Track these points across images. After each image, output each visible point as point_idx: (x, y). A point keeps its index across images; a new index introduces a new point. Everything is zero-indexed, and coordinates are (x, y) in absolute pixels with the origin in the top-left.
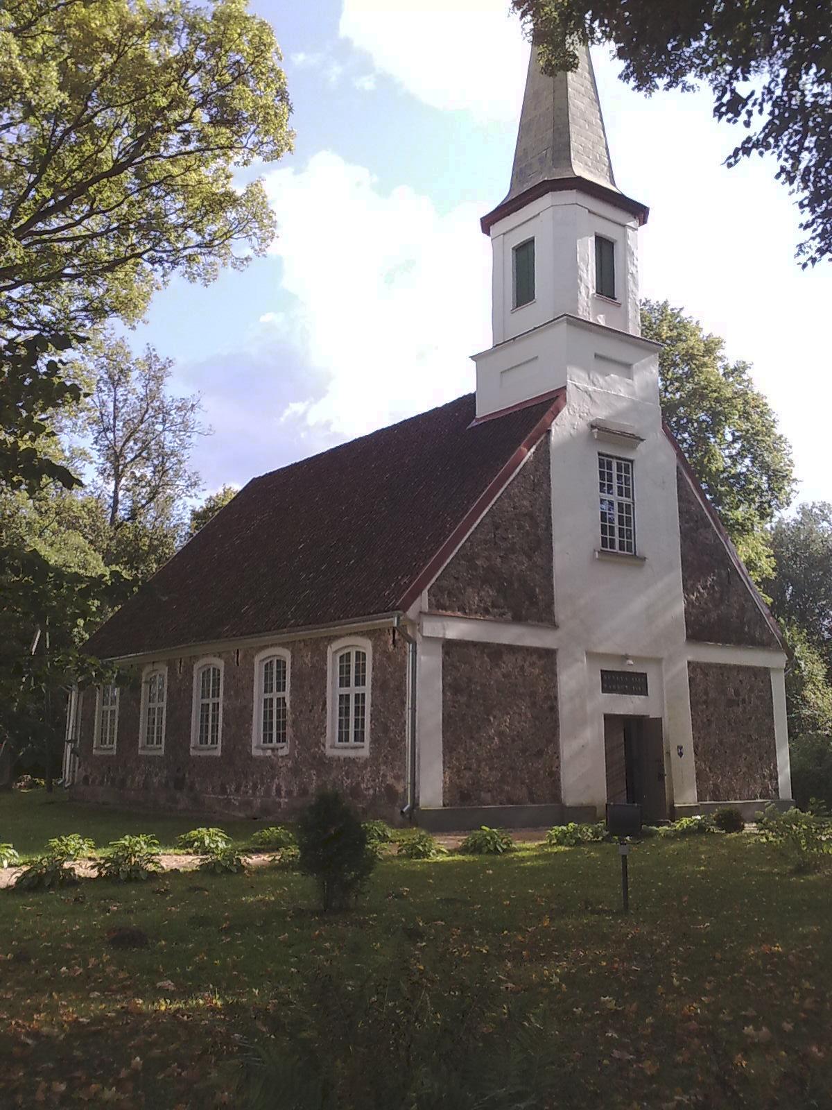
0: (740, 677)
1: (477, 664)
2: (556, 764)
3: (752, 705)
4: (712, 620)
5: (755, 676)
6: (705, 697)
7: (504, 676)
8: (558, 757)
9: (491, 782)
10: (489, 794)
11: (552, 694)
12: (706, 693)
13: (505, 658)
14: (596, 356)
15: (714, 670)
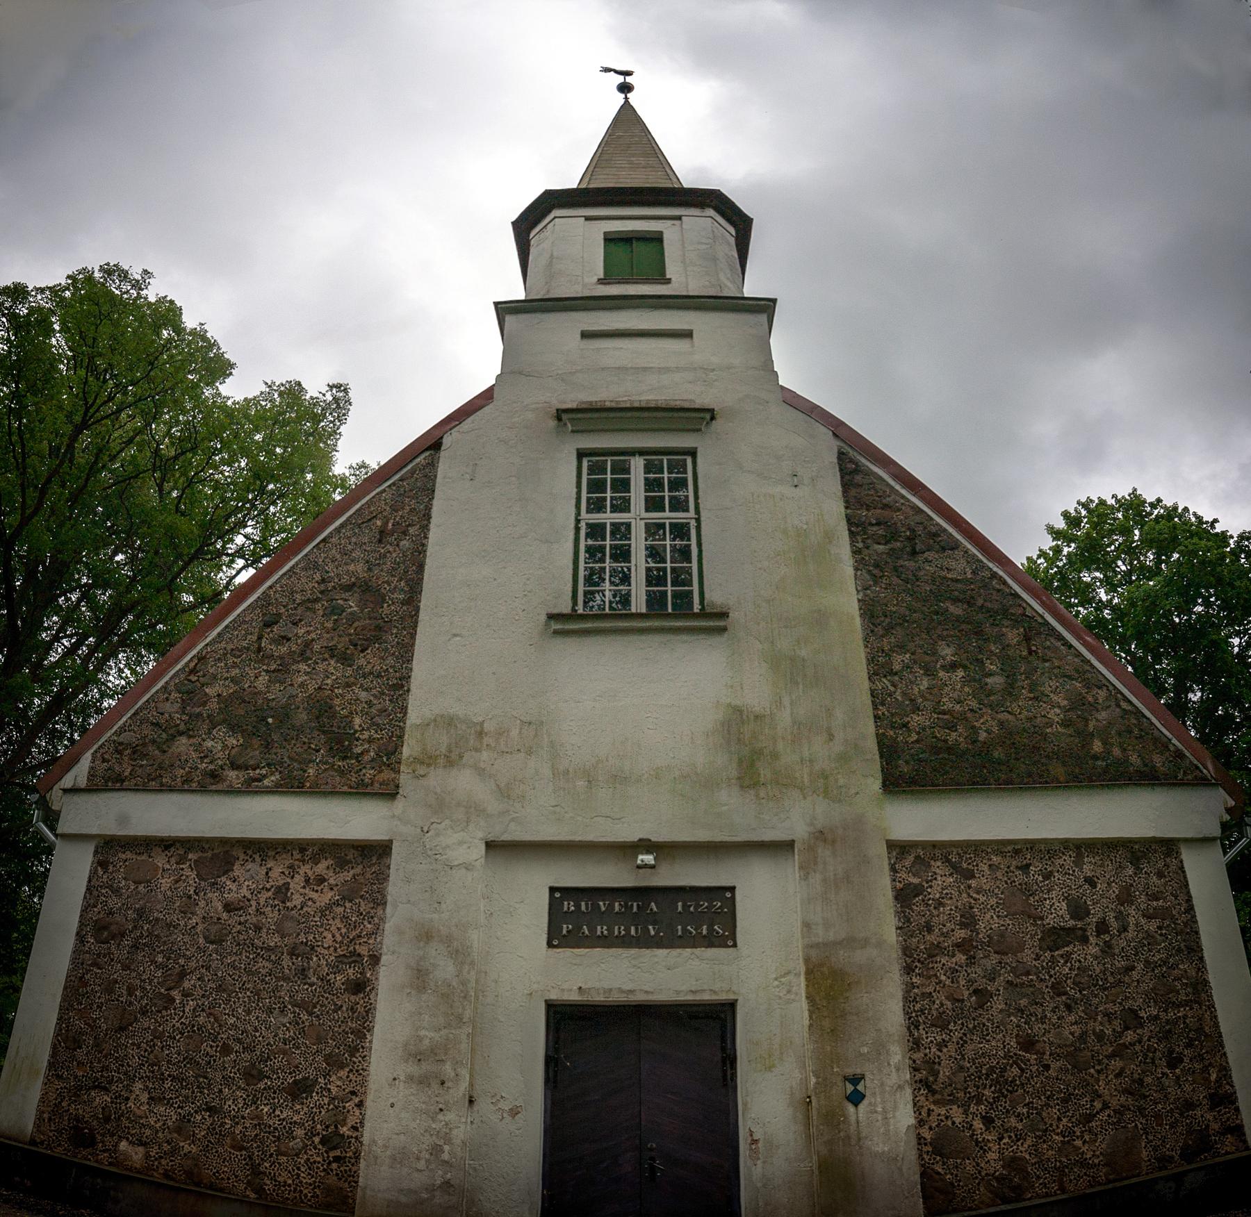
0: (1088, 870)
1: (166, 883)
2: (351, 1121)
3: (1131, 934)
4: (983, 736)
5: (1135, 860)
6: (961, 934)
7: (228, 907)
8: (360, 1105)
9: (151, 1127)
10: (141, 1149)
11: (363, 950)
12: (968, 921)
13: (237, 871)
14: (490, 845)
15: (996, 859)
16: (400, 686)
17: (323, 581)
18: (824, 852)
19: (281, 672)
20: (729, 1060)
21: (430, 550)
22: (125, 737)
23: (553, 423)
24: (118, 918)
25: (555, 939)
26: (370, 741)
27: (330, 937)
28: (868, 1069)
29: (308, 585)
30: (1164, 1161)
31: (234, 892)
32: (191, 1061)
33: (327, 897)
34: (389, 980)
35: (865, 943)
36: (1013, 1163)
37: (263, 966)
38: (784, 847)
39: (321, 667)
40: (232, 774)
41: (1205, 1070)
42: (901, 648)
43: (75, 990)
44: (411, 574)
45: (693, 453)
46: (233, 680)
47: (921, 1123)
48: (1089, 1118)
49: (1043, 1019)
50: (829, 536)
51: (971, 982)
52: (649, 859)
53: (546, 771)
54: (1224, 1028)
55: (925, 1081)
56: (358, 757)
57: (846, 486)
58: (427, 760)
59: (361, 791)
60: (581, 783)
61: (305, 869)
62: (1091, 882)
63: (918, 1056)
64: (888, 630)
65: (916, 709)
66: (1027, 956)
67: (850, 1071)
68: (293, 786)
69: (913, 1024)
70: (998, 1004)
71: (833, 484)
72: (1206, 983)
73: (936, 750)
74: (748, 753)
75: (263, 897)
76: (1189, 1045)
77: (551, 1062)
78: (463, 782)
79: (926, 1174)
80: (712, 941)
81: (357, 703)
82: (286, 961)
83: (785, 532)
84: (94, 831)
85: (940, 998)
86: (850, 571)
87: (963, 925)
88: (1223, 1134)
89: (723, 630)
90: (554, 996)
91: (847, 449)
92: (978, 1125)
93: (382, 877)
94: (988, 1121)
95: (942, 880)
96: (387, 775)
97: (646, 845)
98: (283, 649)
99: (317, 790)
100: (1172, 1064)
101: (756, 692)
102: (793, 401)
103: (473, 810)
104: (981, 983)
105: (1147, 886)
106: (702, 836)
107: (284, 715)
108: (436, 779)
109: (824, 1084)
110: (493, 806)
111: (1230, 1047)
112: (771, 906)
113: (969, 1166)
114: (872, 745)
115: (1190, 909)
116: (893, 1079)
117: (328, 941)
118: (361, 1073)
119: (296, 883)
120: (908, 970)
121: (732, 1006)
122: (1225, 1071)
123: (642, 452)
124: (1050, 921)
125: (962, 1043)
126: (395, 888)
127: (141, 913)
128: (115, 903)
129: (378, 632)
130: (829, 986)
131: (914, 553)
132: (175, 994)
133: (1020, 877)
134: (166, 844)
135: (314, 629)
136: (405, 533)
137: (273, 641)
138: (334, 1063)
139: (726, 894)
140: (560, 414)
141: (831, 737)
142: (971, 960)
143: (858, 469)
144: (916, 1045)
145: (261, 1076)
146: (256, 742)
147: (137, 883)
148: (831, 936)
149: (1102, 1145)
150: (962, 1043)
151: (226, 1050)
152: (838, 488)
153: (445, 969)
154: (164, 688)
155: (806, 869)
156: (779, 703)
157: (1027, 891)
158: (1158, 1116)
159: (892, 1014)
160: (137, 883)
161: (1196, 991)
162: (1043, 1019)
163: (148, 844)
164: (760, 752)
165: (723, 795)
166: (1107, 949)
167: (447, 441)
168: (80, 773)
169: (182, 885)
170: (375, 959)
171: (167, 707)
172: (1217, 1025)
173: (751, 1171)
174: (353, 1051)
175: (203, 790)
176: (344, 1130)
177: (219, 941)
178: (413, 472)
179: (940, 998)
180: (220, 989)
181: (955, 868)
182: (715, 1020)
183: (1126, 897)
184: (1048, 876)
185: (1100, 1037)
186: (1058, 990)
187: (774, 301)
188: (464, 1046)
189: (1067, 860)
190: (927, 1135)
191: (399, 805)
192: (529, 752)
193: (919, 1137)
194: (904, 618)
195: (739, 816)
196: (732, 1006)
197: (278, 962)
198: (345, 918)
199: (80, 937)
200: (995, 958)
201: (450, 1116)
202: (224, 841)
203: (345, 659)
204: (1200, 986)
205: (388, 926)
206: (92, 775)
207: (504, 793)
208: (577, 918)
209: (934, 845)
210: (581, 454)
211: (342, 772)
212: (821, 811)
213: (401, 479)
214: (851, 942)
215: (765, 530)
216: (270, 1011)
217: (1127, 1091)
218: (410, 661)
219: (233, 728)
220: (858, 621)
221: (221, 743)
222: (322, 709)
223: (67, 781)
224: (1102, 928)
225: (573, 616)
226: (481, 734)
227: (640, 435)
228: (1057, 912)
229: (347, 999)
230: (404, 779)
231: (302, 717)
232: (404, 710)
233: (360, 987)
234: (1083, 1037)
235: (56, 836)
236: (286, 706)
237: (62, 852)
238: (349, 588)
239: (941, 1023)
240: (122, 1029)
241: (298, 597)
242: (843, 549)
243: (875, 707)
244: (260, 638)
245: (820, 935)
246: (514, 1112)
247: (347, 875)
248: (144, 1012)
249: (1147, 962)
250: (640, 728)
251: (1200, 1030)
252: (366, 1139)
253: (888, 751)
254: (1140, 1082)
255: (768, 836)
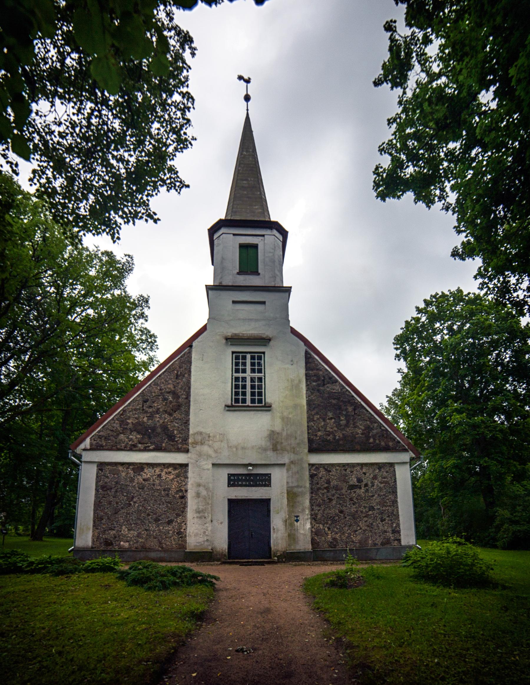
0: (364, 471)
1: (123, 474)
5: (380, 468)
6: (326, 485)
11: (183, 489)
12: (328, 482)
13: (146, 471)
14: (213, 465)
16: (187, 423)
17: (160, 390)
18: (292, 466)
19: (151, 417)
20: (269, 511)
21: (192, 383)
22: (101, 433)
23: (224, 341)
24: (109, 484)
25: (229, 485)
26: (180, 437)
27: (174, 486)
28: (300, 515)
29: (156, 390)
30: (375, 545)
31: (145, 476)
32: (139, 519)
33: (172, 477)
34: (190, 495)
35: (301, 487)
36: (334, 539)
37: (156, 494)
38: (283, 465)
39: (163, 416)
40: (140, 445)
41: (392, 523)
42: (317, 413)
43: (98, 505)
44: (187, 390)
45: (264, 353)
46: (136, 418)
47: (312, 527)
48: (356, 531)
49: (346, 506)
50: (300, 381)
51: (327, 496)
52: (251, 468)
53: (226, 446)
54: (400, 513)
55: (314, 518)
56: (176, 441)
57: (306, 363)
58: (195, 443)
59: (179, 450)
60: (235, 449)
61: (165, 470)
62: (365, 474)
63: (313, 512)
64: (314, 409)
65: (319, 430)
66: (343, 491)
67: (296, 515)
68: (158, 449)
69: (312, 505)
70: (334, 502)
71: (303, 363)
72: (397, 501)
73: (323, 441)
74: (275, 441)
75: (154, 477)
76: (388, 516)
77: (229, 511)
78: (205, 449)
79: (313, 540)
80: (265, 486)
81: (174, 426)
82: (163, 492)
83: (288, 380)
84: (97, 460)
85: (319, 500)
86: (305, 392)
87: (327, 483)
88: (395, 540)
89: (270, 410)
90: (230, 498)
91: (308, 350)
92: (326, 529)
93: (186, 472)
94: (329, 529)
95: (322, 472)
96: (185, 446)
97: (250, 465)
98: (151, 410)
99: (165, 450)
100: (382, 521)
101: (278, 426)
102: (294, 332)
103: (209, 456)
104: (330, 497)
105: (382, 475)
106: (263, 462)
107: (154, 429)
108: (198, 448)
109: (290, 517)
110: (213, 455)
111: (401, 518)
112: (279, 477)
113: (323, 538)
114: (306, 440)
115: (395, 481)
116: (306, 517)
117: (174, 487)
118: (185, 517)
119: (163, 474)
120: (312, 493)
121: (269, 500)
122: (398, 525)
123: (250, 353)
124: (351, 483)
125: (324, 510)
126: (190, 474)
127: (117, 483)
128: (106, 480)
129: (179, 406)
130: (292, 496)
131: (324, 385)
132: (131, 503)
133: (344, 472)
134: (122, 464)
135: (159, 405)
136: (184, 376)
137: (147, 407)
138: (178, 515)
139: (269, 476)
140: (227, 339)
141: (296, 438)
142: (328, 491)
143: (312, 357)
144: (312, 510)
145: (159, 520)
146: (146, 437)
147: (114, 474)
148: (293, 485)
149: (359, 538)
150: (324, 510)
151: (149, 515)
152: (304, 364)
153: (204, 493)
154: (113, 419)
155: (288, 470)
156: (283, 430)
157: (346, 475)
158: (375, 533)
159: (307, 503)
160: (114, 474)
161: (393, 503)
162: (346, 506)
163: (116, 464)
164: (278, 442)
165: (268, 453)
166: (367, 491)
167: (194, 344)
168: (87, 443)
169: (129, 475)
170: (186, 491)
171: (115, 425)
172: (398, 512)
173: (273, 536)
174: (183, 512)
175: (131, 450)
176: (182, 530)
177: (143, 488)
178: (184, 355)
179: (319, 500)
180: (145, 500)
181: (326, 470)
182: (266, 502)
183: (375, 477)
184: (352, 472)
185: (362, 512)
186: (351, 499)
187: (291, 287)
188: (210, 509)
189: (358, 468)
190: (313, 530)
191: (189, 455)
192: (222, 441)
193: (312, 531)
194: (319, 405)
195: (272, 457)
196: (269, 500)
197: (161, 493)
198: (177, 481)
199: (97, 490)
200: (334, 491)
201: (207, 525)
202: (140, 463)
203: (170, 415)
204: (395, 502)
205: (189, 483)
206: (91, 444)
207: (216, 451)
208: (234, 481)
209: (321, 464)
210: (233, 353)
211: (172, 445)
212: (293, 457)
213: (181, 357)
214: (298, 487)
215: (283, 380)
216: (160, 504)
217: (368, 526)
218: (189, 416)
219: (139, 433)
220: (305, 407)
221: (135, 437)
222: (165, 428)
223: (82, 446)
224: (366, 485)
225: (232, 406)
226: (209, 437)
227: (249, 347)
228: (353, 480)
229: (180, 501)
230: (190, 447)
231: (159, 430)
232: (188, 429)
233: (183, 497)
234: (357, 512)
235: (81, 462)
236: (154, 427)
237: (84, 468)
238: (169, 393)
239: (319, 505)
240: (116, 513)
241: (154, 394)
242: (303, 386)
243: (308, 430)
244: (143, 406)
245: (290, 485)
246: (221, 523)
247: (177, 472)
248: (122, 508)
249: (379, 495)
250: (248, 431)
251: (392, 513)
252: (188, 532)
253: (310, 441)
254: (372, 524)
255: (279, 462)
